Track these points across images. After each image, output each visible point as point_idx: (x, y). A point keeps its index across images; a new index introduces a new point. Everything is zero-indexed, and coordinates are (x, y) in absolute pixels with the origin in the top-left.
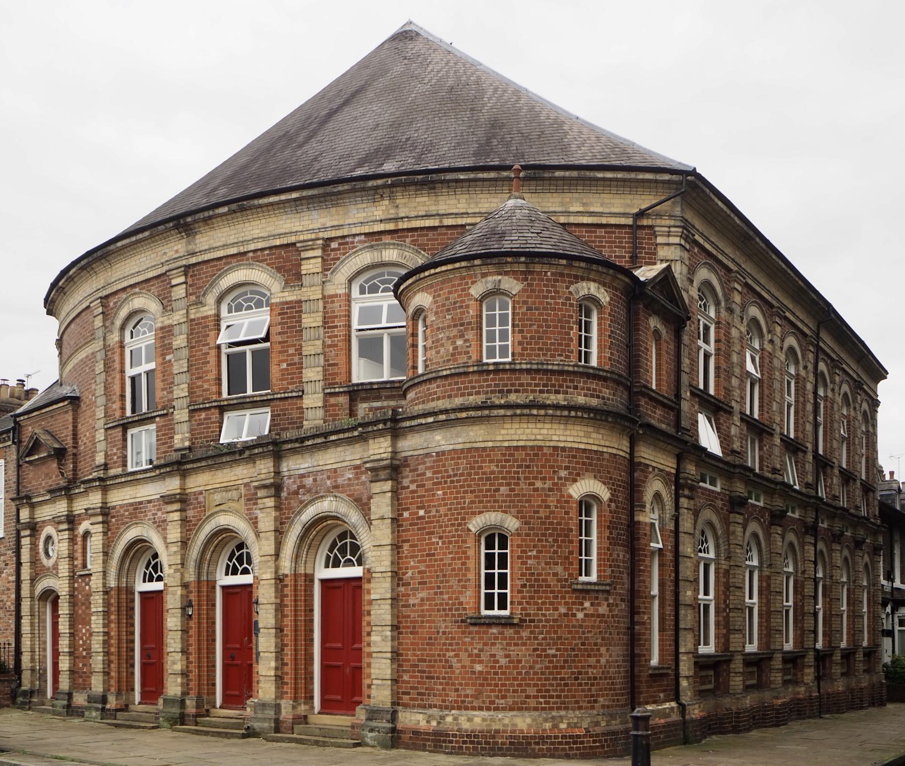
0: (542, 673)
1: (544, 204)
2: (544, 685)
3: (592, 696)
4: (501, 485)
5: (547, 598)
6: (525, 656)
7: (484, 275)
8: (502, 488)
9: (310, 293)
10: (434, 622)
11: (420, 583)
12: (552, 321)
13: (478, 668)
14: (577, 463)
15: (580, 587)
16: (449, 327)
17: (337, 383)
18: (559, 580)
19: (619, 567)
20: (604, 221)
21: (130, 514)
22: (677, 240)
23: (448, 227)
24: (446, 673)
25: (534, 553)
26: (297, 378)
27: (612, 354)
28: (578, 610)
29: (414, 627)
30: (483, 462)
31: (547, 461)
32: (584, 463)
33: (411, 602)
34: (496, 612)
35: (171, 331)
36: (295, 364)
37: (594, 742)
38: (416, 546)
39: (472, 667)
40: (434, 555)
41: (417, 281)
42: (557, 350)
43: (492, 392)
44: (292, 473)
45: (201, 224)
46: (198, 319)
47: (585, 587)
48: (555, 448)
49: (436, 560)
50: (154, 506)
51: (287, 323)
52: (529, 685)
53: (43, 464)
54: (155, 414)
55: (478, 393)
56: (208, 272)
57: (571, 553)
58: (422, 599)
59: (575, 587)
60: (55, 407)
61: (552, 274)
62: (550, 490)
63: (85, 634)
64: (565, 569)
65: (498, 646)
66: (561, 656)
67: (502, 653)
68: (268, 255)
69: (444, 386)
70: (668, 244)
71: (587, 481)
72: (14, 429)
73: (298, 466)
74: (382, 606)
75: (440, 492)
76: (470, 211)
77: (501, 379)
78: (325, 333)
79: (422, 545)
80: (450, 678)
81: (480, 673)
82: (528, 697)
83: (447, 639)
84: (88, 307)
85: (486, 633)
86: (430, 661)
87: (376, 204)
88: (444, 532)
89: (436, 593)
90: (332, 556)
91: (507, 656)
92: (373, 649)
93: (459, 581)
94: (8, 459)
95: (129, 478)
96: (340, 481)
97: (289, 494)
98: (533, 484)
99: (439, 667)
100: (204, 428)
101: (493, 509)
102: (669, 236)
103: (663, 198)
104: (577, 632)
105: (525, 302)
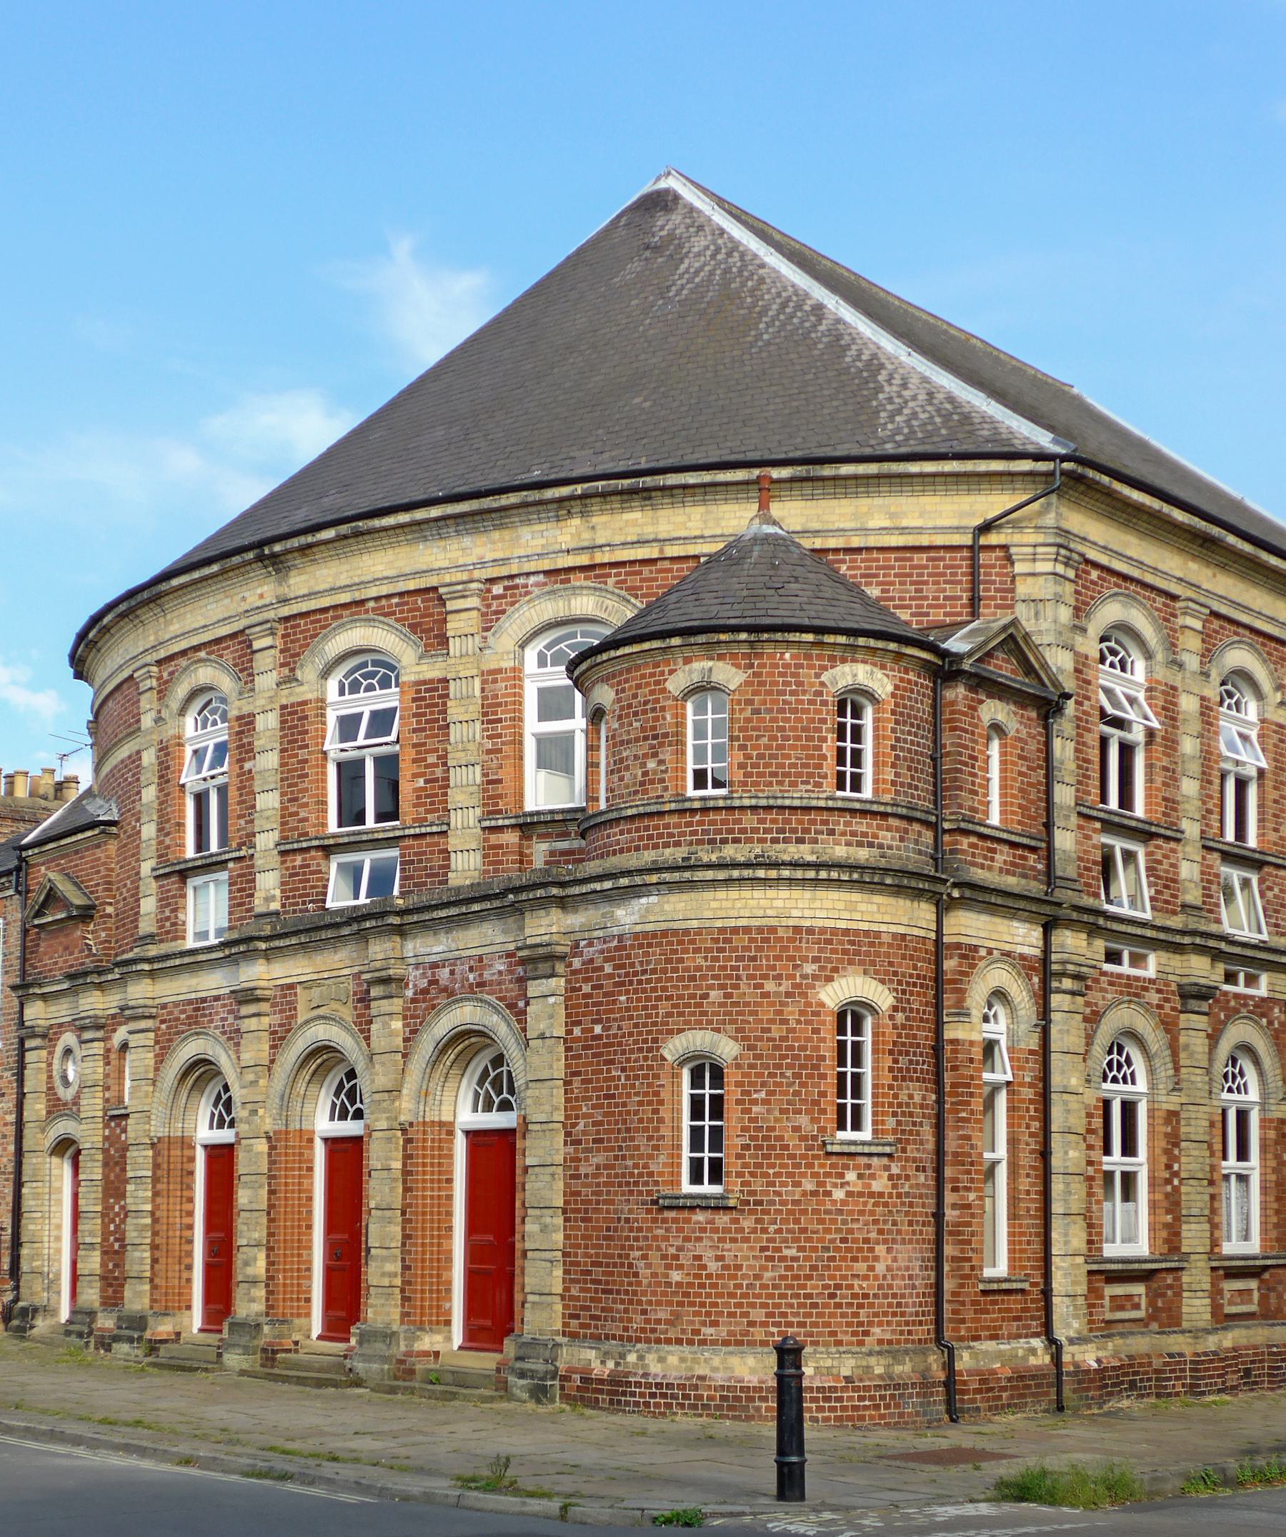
0: (775, 1287)
1: (825, 518)
2: (778, 1306)
3: (861, 1324)
4: (711, 987)
5: (782, 1166)
6: (747, 1258)
7: (687, 661)
8: (713, 993)
9: (461, 668)
10: (612, 1202)
11: (595, 1141)
12: (793, 729)
13: (676, 1276)
14: (834, 951)
15: (836, 1149)
16: (637, 740)
17: (500, 812)
18: (802, 1138)
19: (911, 1115)
20: (924, 540)
21: (189, 1017)
22: (1048, 567)
23: (673, 559)
24: (630, 1284)
25: (763, 1095)
26: (440, 802)
27: (897, 775)
28: (835, 1185)
29: (586, 1211)
30: (685, 951)
31: (786, 949)
32: (845, 952)
33: (582, 1171)
34: (707, 1188)
35: (252, 723)
36: (436, 780)
37: (861, 1398)
38: (590, 1081)
39: (667, 1276)
40: (613, 1096)
41: (592, 667)
42: (799, 775)
43: (700, 842)
44: (421, 959)
45: (296, 554)
46: (293, 705)
47: (846, 1149)
48: (797, 929)
49: (617, 1105)
50: (224, 1006)
51: (424, 714)
52: (753, 1305)
53: (61, 930)
54: (227, 856)
55: (677, 844)
56: (308, 630)
57: (823, 1094)
58: (598, 1167)
59: (829, 1148)
60: (80, 836)
61: (792, 657)
62: (788, 995)
63: (118, 1214)
64: (813, 1120)
65: (705, 1242)
66: (806, 1259)
67: (710, 1254)
68: (397, 605)
69: (629, 831)
70: (1033, 575)
71: (850, 979)
72: (18, 869)
73: (428, 950)
74: (541, 1177)
75: (623, 998)
76: (707, 533)
77: (712, 823)
78: (483, 730)
79: (598, 1080)
80: (635, 1293)
81: (679, 1284)
82: (752, 1324)
83: (631, 1230)
84: (131, 677)
85: (688, 1221)
86: (608, 1265)
87: (563, 524)
88: (628, 1060)
89: (616, 1158)
90: (482, 1092)
91: (719, 1258)
92: (528, 1245)
93: (650, 1138)
94: (9, 917)
95: (187, 960)
96: (487, 975)
97: (415, 993)
98: (761, 986)
99: (619, 1275)
100: (301, 881)
101: (699, 1025)
102: (1034, 560)
103: (1025, 498)
104: (834, 1221)
105: (749, 702)
